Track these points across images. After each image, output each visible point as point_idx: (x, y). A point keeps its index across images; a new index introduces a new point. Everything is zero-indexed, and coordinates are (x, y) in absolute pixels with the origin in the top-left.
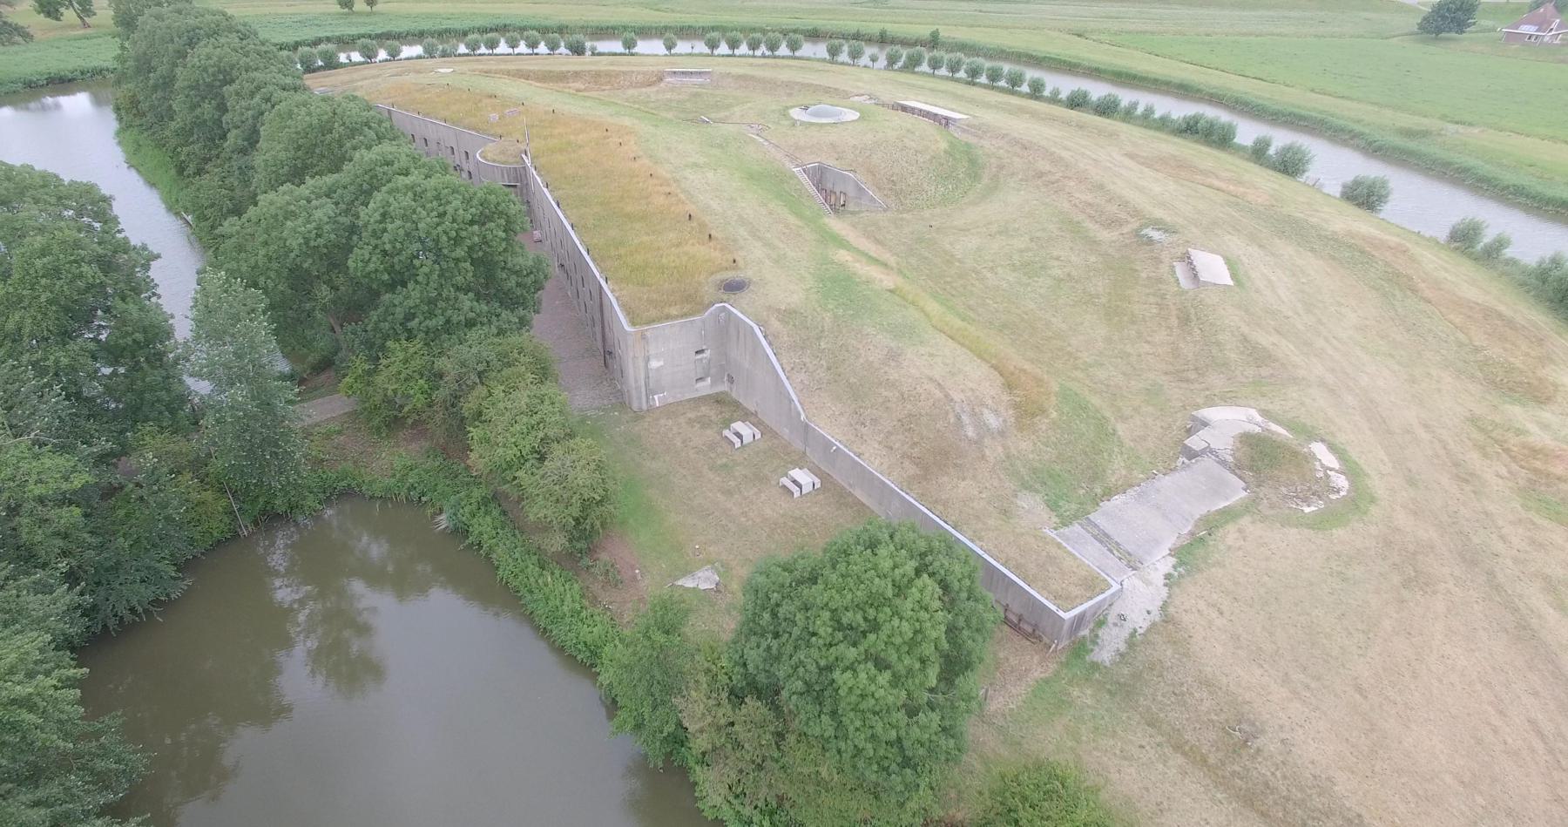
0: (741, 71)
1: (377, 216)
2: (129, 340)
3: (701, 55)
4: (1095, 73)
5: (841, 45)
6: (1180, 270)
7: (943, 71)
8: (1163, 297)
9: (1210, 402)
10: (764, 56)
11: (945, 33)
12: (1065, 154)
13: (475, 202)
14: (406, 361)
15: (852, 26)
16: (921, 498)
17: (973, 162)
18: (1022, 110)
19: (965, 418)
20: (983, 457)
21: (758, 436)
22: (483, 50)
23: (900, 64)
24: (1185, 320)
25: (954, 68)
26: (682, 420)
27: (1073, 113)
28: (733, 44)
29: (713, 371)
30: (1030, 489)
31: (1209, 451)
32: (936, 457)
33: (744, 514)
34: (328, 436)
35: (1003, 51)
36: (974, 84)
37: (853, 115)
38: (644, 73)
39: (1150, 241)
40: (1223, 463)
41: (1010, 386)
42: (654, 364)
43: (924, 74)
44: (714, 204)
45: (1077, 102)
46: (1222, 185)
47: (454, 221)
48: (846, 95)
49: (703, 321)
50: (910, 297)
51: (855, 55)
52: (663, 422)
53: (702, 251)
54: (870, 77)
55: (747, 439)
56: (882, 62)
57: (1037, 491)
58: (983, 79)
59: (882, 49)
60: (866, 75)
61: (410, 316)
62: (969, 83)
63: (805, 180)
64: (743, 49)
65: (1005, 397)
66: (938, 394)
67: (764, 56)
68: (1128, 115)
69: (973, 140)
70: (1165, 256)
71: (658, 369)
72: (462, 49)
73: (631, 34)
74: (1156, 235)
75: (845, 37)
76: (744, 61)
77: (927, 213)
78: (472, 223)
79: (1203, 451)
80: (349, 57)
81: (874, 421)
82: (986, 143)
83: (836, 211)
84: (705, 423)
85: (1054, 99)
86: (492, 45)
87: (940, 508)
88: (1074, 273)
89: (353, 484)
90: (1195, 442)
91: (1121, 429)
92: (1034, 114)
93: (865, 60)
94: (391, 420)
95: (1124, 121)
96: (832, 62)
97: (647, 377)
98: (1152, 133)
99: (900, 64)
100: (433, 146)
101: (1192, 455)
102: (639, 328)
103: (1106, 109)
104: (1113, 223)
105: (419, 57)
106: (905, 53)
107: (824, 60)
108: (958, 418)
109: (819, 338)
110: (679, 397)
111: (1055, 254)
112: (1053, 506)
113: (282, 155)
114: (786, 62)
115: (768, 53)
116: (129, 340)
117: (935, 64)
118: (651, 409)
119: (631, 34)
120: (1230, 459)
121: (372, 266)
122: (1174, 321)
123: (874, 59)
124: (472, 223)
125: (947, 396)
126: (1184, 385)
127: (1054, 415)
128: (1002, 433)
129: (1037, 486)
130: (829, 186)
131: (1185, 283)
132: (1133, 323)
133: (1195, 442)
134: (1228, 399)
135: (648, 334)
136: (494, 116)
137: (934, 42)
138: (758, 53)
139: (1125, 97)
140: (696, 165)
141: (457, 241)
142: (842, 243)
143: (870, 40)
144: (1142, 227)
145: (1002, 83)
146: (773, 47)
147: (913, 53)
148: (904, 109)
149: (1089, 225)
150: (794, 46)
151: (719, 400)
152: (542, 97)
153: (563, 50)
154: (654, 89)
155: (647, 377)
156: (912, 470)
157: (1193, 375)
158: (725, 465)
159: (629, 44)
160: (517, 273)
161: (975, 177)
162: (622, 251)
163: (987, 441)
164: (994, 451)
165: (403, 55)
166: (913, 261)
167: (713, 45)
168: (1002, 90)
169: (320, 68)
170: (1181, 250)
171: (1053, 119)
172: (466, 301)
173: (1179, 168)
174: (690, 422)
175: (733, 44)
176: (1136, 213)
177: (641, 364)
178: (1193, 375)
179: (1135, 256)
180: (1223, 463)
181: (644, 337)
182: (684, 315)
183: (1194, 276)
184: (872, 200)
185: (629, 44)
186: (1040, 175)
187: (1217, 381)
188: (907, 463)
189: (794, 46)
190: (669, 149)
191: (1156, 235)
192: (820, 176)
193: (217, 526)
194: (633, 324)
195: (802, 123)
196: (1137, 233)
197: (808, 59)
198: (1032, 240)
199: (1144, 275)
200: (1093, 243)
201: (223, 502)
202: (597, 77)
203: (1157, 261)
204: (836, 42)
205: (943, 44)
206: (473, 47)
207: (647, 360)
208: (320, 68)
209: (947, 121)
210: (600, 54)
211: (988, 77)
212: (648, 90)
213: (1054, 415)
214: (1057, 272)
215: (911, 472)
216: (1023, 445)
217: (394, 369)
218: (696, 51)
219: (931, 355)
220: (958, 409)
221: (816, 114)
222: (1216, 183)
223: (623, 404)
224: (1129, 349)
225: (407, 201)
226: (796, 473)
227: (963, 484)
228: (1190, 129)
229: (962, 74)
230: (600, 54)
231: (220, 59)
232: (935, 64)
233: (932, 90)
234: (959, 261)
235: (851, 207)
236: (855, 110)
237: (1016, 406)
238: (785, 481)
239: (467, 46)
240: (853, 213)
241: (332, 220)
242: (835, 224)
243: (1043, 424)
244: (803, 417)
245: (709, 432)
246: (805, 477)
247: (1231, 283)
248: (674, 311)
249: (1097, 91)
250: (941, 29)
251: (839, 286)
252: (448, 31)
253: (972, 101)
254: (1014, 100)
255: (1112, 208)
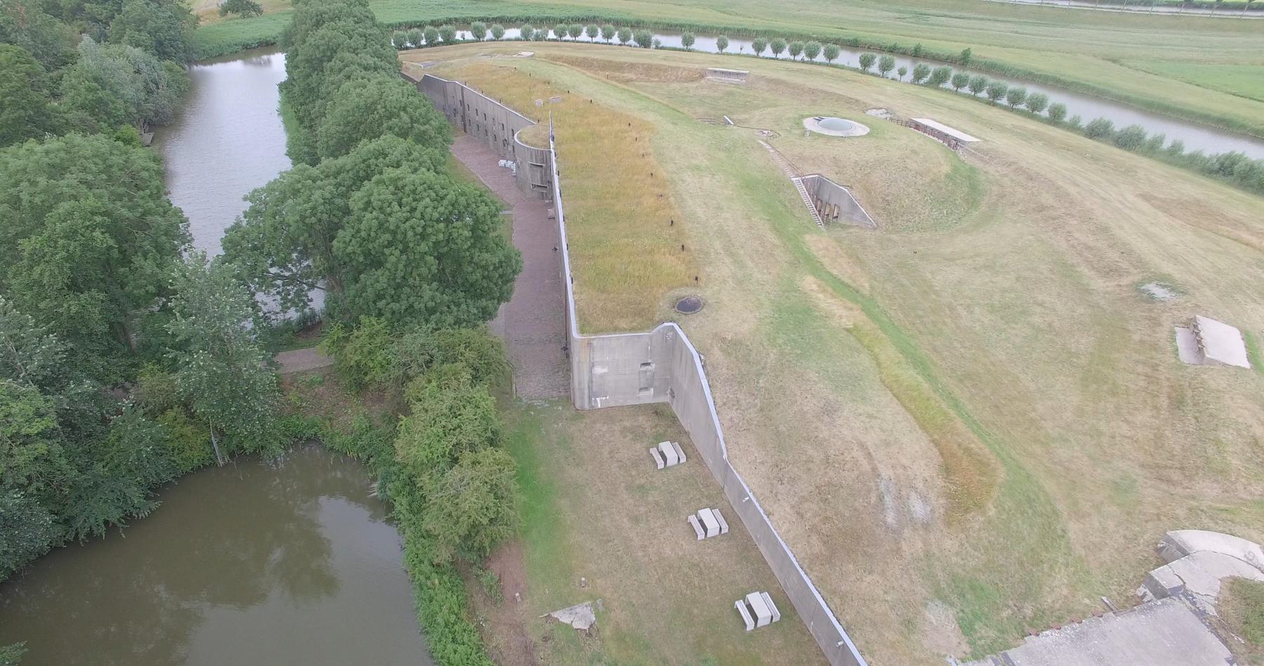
0: (774, 75)
1: (361, 205)
2: (142, 292)
3: (748, 56)
4: (1123, 101)
5: (873, 58)
6: (1182, 338)
7: (966, 90)
8: (1155, 367)
9: (1197, 519)
10: (803, 61)
11: (977, 52)
12: (1072, 190)
13: (445, 202)
14: (371, 336)
15: (890, 39)
16: (820, 582)
17: (973, 188)
18: (1037, 136)
19: (888, 500)
20: (898, 551)
21: (683, 460)
22: (568, 37)
23: (926, 79)
24: (1177, 402)
25: (977, 87)
26: (617, 428)
27: (1090, 144)
28: (777, 49)
29: (656, 384)
30: (944, 599)
31: (1181, 592)
32: (847, 537)
33: (644, 548)
34: (311, 384)
35: (1030, 74)
36: (995, 105)
37: (862, 130)
38: (690, 70)
39: (1151, 298)
40: (1201, 614)
41: (947, 470)
42: (598, 370)
43: (947, 90)
44: (700, 212)
45: (1097, 132)
46: (1254, 240)
47: (423, 217)
48: (865, 108)
49: (651, 338)
50: (866, 341)
51: (886, 67)
52: (598, 425)
53: (670, 263)
54: (895, 91)
55: (672, 460)
56: (909, 76)
57: (952, 605)
58: (1004, 101)
59: (914, 62)
60: (890, 88)
61: (379, 297)
62: (989, 103)
63: (802, 190)
64: (786, 54)
65: (940, 482)
66: (866, 466)
67: (803, 61)
68: (1152, 149)
69: (978, 164)
70: (1166, 319)
71: (602, 376)
72: (551, 35)
73: (689, 31)
74: (1160, 293)
75: (881, 49)
76: (779, 66)
77: (915, 237)
78: (438, 221)
79: (1175, 592)
80: (463, 36)
81: (793, 480)
82: (991, 169)
83: (827, 223)
84: (637, 434)
85: (1073, 127)
86: (576, 33)
87: (837, 601)
88: (1056, 324)
89: (319, 434)
90: (1165, 575)
91: (1073, 527)
92: (1049, 143)
93: (894, 73)
94: (358, 382)
95: (1145, 154)
96: (863, 72)
97: (591, 381)
98: (1177, 171)
99: (926, 79)
100: (490, 120)
101: (1161, 593)
102: (586, 337)
103: (1129, 141)
104: (1109, 272)
105: (517, 39)
106: (932, 67)
107: (856, 70)
108: (881, 498)
109: (759, 375)
110: (621, 402)
111: (1040, 298)
112: (966, 628)
113: (332, 131)
114: (820, 69)
115: (806, 59)
116: (142, 292)
117: (960, 82)
118: (593, 410)
119: (689, 31)
120: (1212, 611)
121: (350, 249)
122: (1164, 402)
123: (902, 73)
124: (438, 221)
125: (874, 469)
126: (1164, 486)
127: (992, 512)
128: (926, 526)
129: (954, 598)
130: (825, 198)
131: (1185, 355)
132: (1114, 394)
133: (1165, 575)
134: (1219, 519)
135: (595, 343)
136: (539, 102)
137: (964, 60)
138: (798, 58)
139: (1152, 128)
140: (698, 168)
141: (423, 236)
142: (816, 268)
143: (904, 53)
144: (1142, 282)
145: (1023, 107)
146: (811, 54)
147: (942, 70)
148: (918, 126)
149: (1084, 270)
150: (831, 55)
151: (658, 411)
152: (586, 85)
153: (632, 42)
154: (695, 84)
155: (591, 381)
156: (817, 546)
157: (1176, 476)
158: (641, 487)
159: (688, 42)
160: (485, 268)
161: (972, 202)
162: (597, 252)
163: (907, 533)
164: (912, 545)
165: (505, 37)
166: (889, 286)
167: (759, 48)
168: (1021, 113)
169: (439, 44)
170: (1186, 315)
171: (1068, 148)
172: (427, 291)
173: (1199, 214)
174: (624, 431)
175: (777, 49)
176: (1140, 264)
177: (585, 368)
178: (1176, 476)
179: (1131, 315)
180: (1201, 614)
181: (590, 344)
182: (632, 330)
183: (1200, 349)
184: (864, 217)
185: (688, 42)
186: (1041, 208)
187: (1208, 490)
188: (814, 538)
189: (831, 55)
190: (678, 148)
191: (1160, 293)
192: (818, 189)
193: (196, 456)
194: (582, 331)
195: (812, 133)
196: (1137, 287)
197: (842, 67)
198: (1018, 279)
199: (1136, 337)
200: (1085, 291)
201: (204, 437)
202: (650, 71)
203: (1155, 323)
204: (869, 54)
205: (973, 62)
206: (561, 34)
207: (592, 366)
208: (439, 44)
209: (954, 143)
210: (662, 48)
211: (1009, 99)
212: (690, 85)
213: (992, 512)
214: (1036, 320)
215: (816, 550)
216: (948, 544)
217: (358, 343)
218: (744, 52)
219: (870, 416)
220: (882, 487)
221: (827, 127)
222: (1246, 236)
223: (569, 398)
224: (1103, 426)
225: (386, 193)
226: (706, 514)
227: (869, 578)
228: (1225, 170)
229: (984, 94)
230: (662, 48)
231: (330, 39)
232: (960, 82)
233: (950, 108)
234: (936, 293)
235: (842, 220)
236: (872, 125)
237: (949, 496)
238: (693, 519)
239: (556, 33)
240: (844, 227)
241: (327, 201)
242: (818, 242)
243: (976, 521)
244: (725, 456)
245: (638, 446)
246: (712, 519)
247: (1247, 365)
248: (623, 324)
249: (1121, 120)
250: (973, 47)
251: (795, 318)
252: (548, 19)
253: (989, 124)
254: (1032, 125)
255: (1113, 255)
